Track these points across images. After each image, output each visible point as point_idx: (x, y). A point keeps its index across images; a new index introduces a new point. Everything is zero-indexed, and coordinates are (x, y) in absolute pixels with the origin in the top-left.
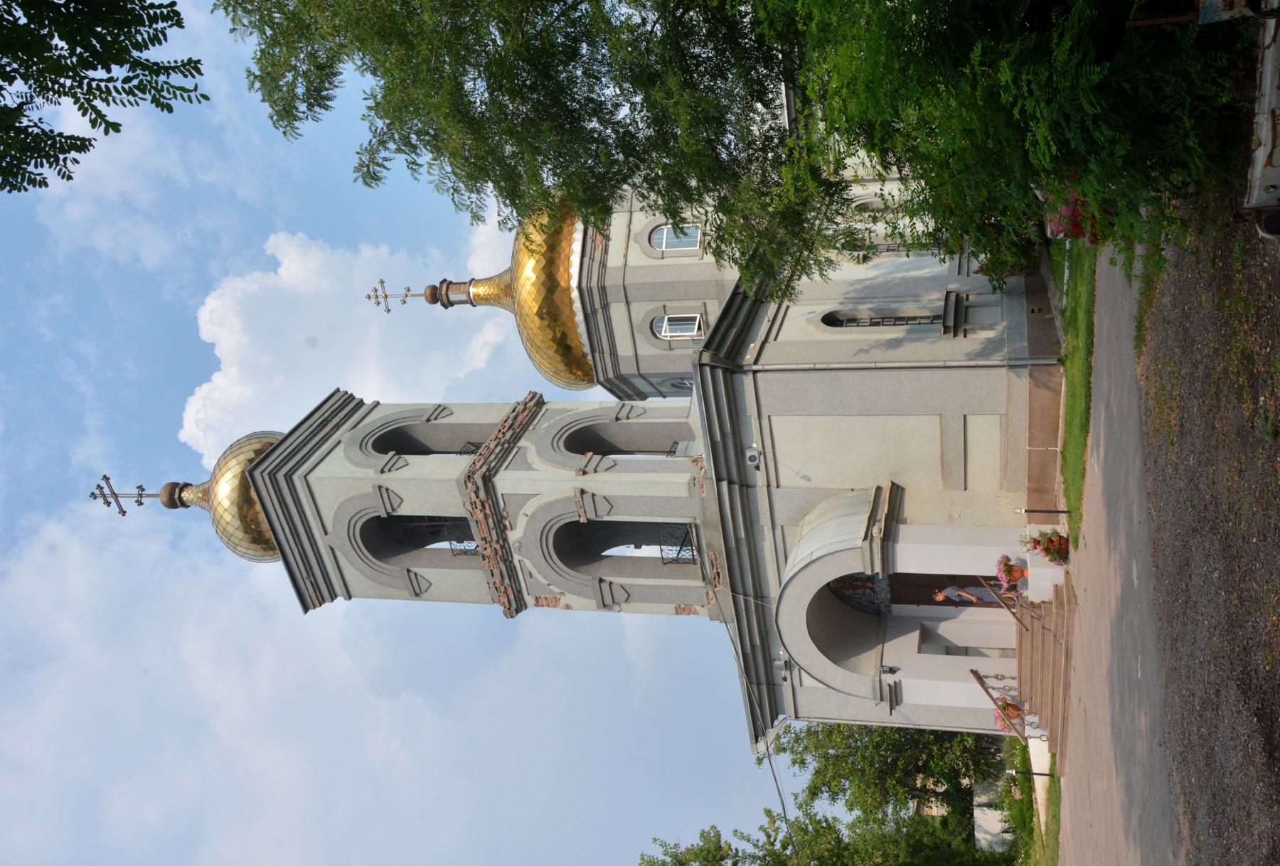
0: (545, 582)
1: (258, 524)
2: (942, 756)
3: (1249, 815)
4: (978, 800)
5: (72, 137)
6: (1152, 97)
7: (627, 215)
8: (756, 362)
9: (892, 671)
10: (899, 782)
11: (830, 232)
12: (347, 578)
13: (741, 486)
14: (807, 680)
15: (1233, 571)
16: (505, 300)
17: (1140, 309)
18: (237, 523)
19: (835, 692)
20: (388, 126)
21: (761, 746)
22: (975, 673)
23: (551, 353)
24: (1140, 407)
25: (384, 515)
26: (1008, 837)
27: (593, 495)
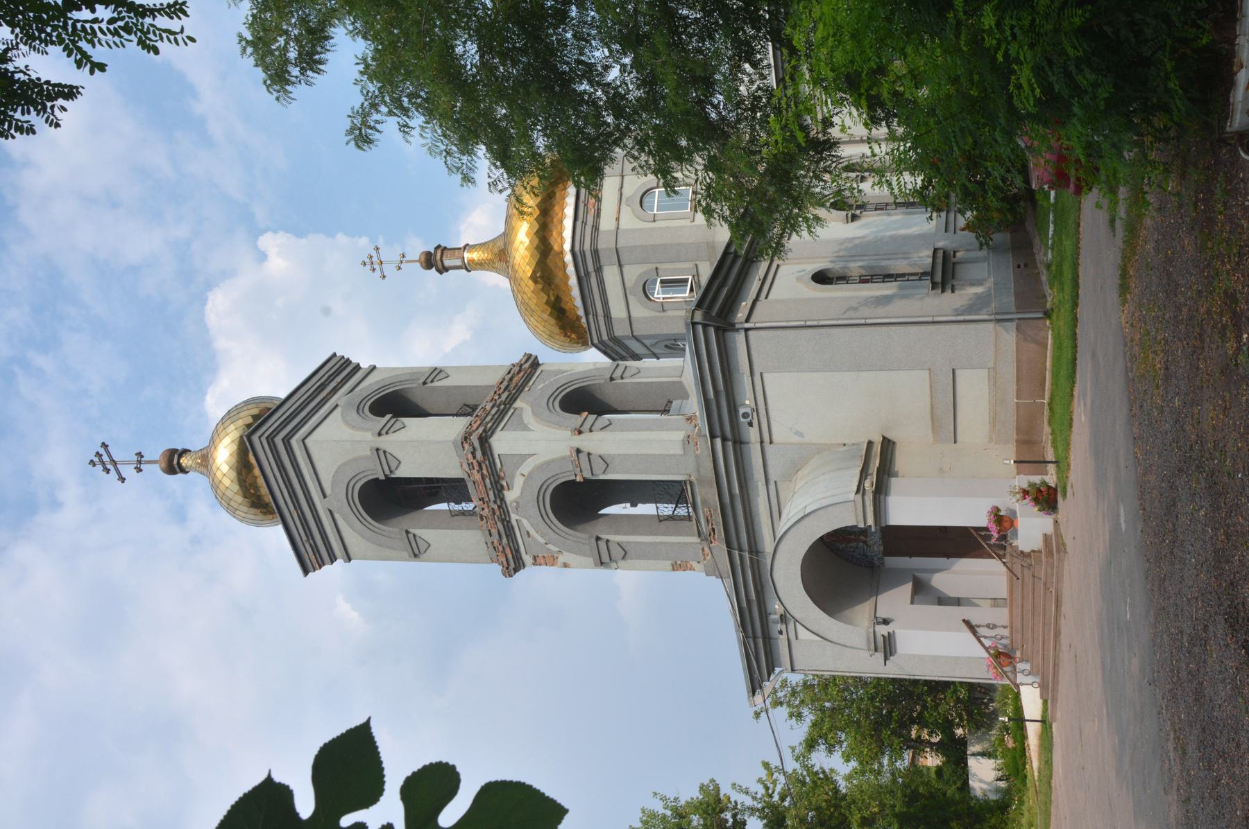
0: (542, 541)
1: (257, 488)
2: (936, 707)
3: (1238, 746)
4: (972, 749)
5: (59, 85)
6: (1133, 40)
7: (618, 179)
8: (747, 321)
9: (886, 622)
10: (894, 732)
11: (818, 190)
12: (347, 541)
13: (735, 442)
14: (803, 633)
15: (1219, 508)
16: (499, 265)
17: (1124, 257)
18: (236, 488)
19: (829, 645)
20: (380, 89)
21: (758, 698)
22: (967, 622)
23: (546, 316)
24: (1125, 354)
25: (382, 477)
26: (1002, 784)
27: (589, 454)
